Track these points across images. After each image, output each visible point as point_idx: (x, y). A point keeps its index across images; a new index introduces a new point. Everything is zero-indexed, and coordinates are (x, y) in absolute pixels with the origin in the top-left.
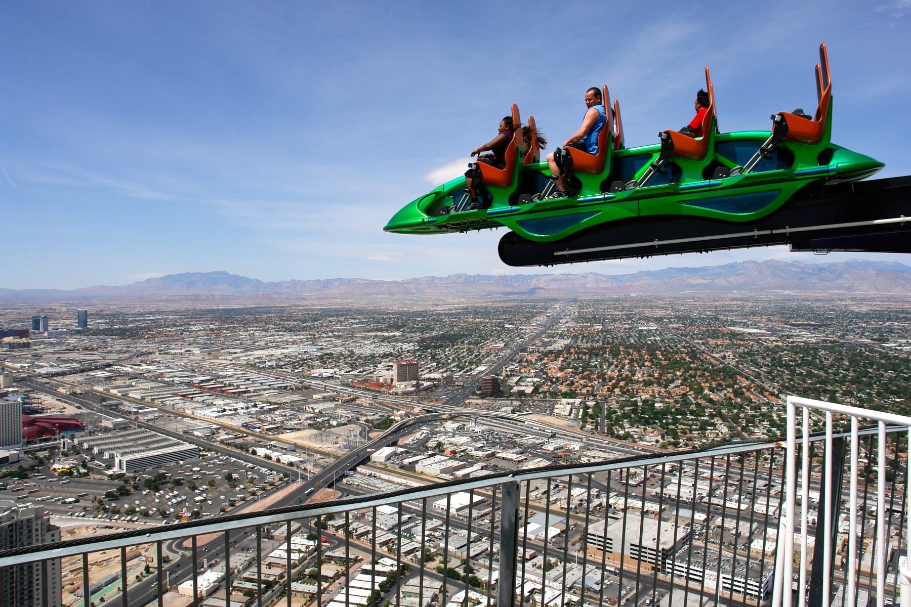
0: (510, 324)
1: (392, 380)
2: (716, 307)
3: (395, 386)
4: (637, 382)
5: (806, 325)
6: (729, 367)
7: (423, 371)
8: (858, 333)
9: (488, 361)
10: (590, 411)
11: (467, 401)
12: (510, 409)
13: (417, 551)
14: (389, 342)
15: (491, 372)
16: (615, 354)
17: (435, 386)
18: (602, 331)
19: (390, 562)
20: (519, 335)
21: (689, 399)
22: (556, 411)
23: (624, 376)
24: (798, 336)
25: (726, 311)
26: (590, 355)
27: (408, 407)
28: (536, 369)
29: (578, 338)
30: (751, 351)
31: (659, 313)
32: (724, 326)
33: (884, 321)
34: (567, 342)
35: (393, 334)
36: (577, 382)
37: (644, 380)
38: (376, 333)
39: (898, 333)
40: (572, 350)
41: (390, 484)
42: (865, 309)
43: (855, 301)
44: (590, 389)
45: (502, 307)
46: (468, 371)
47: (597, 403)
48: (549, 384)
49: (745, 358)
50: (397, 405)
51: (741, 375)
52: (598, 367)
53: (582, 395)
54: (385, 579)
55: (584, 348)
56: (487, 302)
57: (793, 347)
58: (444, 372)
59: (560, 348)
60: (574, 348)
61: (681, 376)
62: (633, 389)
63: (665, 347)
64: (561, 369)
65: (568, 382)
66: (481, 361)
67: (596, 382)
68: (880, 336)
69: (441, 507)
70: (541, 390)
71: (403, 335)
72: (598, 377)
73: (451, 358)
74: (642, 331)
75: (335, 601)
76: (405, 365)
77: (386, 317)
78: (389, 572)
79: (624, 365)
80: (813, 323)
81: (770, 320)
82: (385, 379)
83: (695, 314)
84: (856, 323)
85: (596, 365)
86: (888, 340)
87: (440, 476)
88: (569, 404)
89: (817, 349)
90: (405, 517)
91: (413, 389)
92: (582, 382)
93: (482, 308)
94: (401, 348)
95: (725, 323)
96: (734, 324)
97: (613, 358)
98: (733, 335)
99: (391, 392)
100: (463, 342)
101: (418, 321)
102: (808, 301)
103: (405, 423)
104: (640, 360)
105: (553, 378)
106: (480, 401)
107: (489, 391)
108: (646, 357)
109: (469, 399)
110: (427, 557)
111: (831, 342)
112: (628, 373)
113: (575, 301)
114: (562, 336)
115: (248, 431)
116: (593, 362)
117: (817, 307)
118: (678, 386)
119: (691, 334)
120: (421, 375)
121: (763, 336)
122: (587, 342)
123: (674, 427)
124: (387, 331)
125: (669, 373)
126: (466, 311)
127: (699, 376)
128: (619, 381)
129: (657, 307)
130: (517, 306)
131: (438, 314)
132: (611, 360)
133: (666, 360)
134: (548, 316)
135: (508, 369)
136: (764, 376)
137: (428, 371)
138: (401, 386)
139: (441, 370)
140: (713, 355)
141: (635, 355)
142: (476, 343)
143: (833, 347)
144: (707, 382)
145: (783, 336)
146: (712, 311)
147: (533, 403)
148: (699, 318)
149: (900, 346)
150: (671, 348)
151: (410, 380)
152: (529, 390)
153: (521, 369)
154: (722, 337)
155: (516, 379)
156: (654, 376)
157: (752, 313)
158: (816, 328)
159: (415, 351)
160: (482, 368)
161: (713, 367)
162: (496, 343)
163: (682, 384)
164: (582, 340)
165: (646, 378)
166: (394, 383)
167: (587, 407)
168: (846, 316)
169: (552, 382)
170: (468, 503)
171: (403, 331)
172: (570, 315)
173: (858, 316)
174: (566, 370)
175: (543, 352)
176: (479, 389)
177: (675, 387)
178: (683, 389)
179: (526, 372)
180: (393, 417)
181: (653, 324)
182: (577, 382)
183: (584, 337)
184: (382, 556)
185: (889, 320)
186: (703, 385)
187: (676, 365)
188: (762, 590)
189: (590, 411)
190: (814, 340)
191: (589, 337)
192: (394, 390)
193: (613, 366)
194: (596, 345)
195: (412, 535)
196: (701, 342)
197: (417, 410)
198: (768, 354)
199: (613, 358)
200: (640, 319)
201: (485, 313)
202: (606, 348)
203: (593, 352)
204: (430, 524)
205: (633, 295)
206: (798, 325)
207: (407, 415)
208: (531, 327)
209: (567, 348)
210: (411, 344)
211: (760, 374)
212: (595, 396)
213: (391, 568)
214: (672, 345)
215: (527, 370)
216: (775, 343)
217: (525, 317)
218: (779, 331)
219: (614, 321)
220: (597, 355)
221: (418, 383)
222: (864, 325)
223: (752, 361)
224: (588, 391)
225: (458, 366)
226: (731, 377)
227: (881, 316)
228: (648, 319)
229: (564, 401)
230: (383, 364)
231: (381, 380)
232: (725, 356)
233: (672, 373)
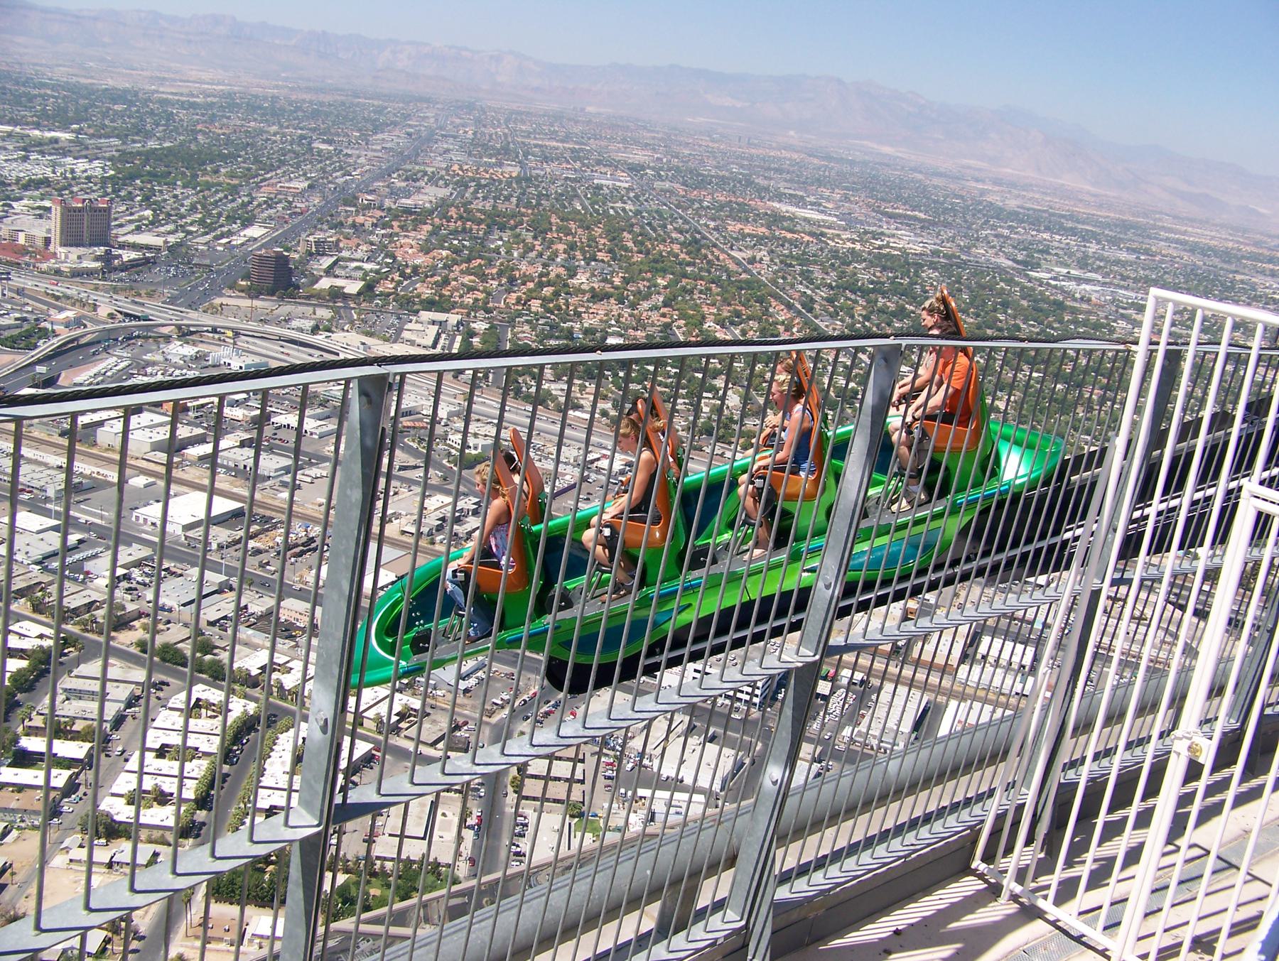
0: (324, 142)
1: (47, 241)
2: (751, 158)
3: (54, 255)
4: (581, 291)
5: (910, 218)
6: (759, 281)
7: (121, 226)
8: (993, 247)
9: (270, 218)
10: (476, 341)
11: (217, 301)
12: (308, 324)
13: (98, 608)
14: (42, 153)
15: (275, 241)
16: (540, 230)
17: (146, 261)
18: (519, 180)
19: (36, 629)
20: (341, 168)
21: (675, 334)
22: (406, 335)
23: (552, 275)
24: (893, 236)
25: (769, 169)
26: (489, 226)
27: (84, 305)
28: (372, 244)
29: (467, 187)
30: (804, 253)
31: (639, 156)
32: (762, 198)
33: (1038, 231)
34: (443, 192)
35: (53, 134)
36: (456, 279)
37: (593, 288)
38: (8, 128)
39: (1056, 254)
40: (453, 212)
41: (38, 469)
42: (1012, 204)
43: (1000, 185)
44: (481, 296)
45: (311, 102)
46: (222, 236)
47: (492, 327)
48: (397, 278)
49: (791, 265)
50: (57, 298)
51: (777, 297)
52: (503, 251)
53: (462, 306)
54: (24, 664)
55: (478, 210)
56: (277, 87)
57: (880, 256)
58: (170, 233)
59: (427, 205)
60: (457, 207)
61: (665, 287)
62: (567, 305)
63: (642, 227)
64: (426, 249)
65: (438, 278)
66: (254, 216)
67: (495, 283)
68: (1027, 256)
69: (150, 520)
70: (379, 289)
71: (77, 142)
72: (500, 274)
73: (187, 202)
74: (600, 187)
75: (1004, 677)
76: (80, 210)
77: (36, 92)
78: (34, 651)
79: (556, 254)
80: (922, 216)
81: (846, 199)
82: (30, 238)
83: (709, 169)
84: (993, 227)
85: (499, 247)
86: (1039, 265)
87: (151, 456)
88: (434, 323)
89: (922, 266)
90: (73, 538)
91: (97, 265)
92: (467, 279)
93: (265, 99)
94: (73, 171)
95: (762, 192)
96: (779, 197)
97: (535, 238)
98: (775, 219)
99: (44, 266)
100: (216, 172)
101: (116, 112)
102: (920, 172)
103: (76, 339)
104: (589, 246)
105: (407, 266)
106: (246, 303)
107: (269, 283)
108: (602, 241)
109: (222, 295)
110: (121, 623)
111: (945, 256)
112: (562, 271)
113: (470, 107)
114: (433, 180)
115: (822, 714)
116: (493, 241)
117: (935, 187)
118: (656, 308)
119: (696, 205)
120: (117, 236)
121: (829, 228)
122: (485, 198)
123: (639, 387)
124: (37, 126)
125: (643, 280)
126: (230, 103)
127: (701, 292)
128: (541, 285)
129: (636, 142)
130: (343, 104)
131: (164, 102)
132: (529, 240)
133: (640, 252)
134: (410, 135)
135: (311, 238)
136: (821, 305)
137: (132, 227)
138: (69, 257)
139: (162, 229)
140: (733, 253)
141: (581, 236)
142: (248, 176)
143: (950, 267)
144: (713, 305)
145: (866, 232)
146: (742, 166)
147: (359, 314)
148: (717, 177)
149: (1055, 279)
150: (654, 230)
151: (91, 245)
152: (353, 287)
153: (339, 241)
154: (755, 221)
155: (326, 262)
156: (612, 283)
157: (818, 180)
158: (925, 226)
159: (104, 180)
160: (255, 231)
161: (729, 276)
162: (291, 179)
163: (665, 305)
164: (476, 192)
165: (596, 286)
166: (51, 248)
167: (472, 334)
168: (980, 211)
169: (403, 275)
170: (202, 516)
171: (78, 132)
172: (455, 137)
173: (1000, 214)
174: (435, 253)
175: (390, 209)
176: (247, 277)
177: (651, 309)
178: (664, 315)
179: (350, 249)
180: (49, 326)
181: (622, 175)
182: (456, 279)
183: (479, 186)
184: (21, 617)
185: (1047, 229)
186: (705, 309)
187: (658, 265)
188: (758, 692)
189: (476, 341)
190: (918, 249)
191: (491, 188)
192: (52, 263)
193: (532, 255)
194: (502, 207)
195: (88, 573)
196: (712, 224)
197: (103, 311)
198: (833, 265)
199: (535, 238)
200: (599, 163)
201: (274, 112)
202: (523, 215)
203: (496, 221)
204: (125, 554)
205: (590, 109)
206: (890, 216)
207: (78, 322)
208: (370, 154)
209: (443, 204)
210: (96, 163)
211: (812, 300)
212: (488, 311)
213: (39, 642)
214: (655, 223)
215: (352, 243)
216: (849, 245)
217: (359, 130)
218: (861, 223)
219: (546, 159)
220: (502, 228)
221: (108, 253)
222: (1006, 232)
223: (802, 274)
224: (476, 300)
225: (202, 222)
226: (760, 300)
227: (1035, 220)
228: (615, 165)
229: (426, 315)
230: (25, 202)
231: (22, 240)
232: (754, 258)
233: (648, 280)
